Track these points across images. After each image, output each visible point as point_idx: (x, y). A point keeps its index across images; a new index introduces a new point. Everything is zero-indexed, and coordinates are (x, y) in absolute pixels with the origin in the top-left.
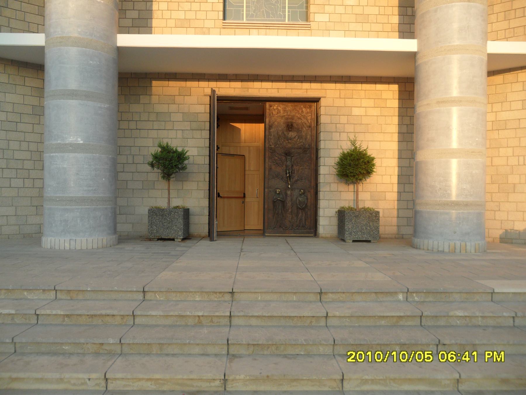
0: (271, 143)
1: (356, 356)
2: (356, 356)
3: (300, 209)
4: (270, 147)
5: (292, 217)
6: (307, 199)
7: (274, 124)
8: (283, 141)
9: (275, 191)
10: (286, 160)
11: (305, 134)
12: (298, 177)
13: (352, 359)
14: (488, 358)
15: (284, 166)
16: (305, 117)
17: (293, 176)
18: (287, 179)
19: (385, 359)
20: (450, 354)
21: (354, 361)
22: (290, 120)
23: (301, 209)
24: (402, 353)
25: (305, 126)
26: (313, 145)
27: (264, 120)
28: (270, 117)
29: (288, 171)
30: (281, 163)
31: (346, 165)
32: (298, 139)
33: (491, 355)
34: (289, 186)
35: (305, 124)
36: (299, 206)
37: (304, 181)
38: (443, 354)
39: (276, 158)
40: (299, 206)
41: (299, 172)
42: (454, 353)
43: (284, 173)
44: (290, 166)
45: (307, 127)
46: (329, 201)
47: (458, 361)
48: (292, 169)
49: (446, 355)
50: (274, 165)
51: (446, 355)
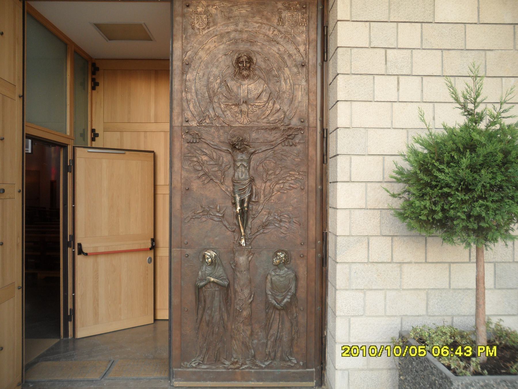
0: (189, 114)
1: (350, 350)
2: (350, 350)
3: (275, 307)
4: (185, 124)
5: (252, 331)
6: (296, 278)
7: (197, 57)
8: (222, 106)
9: (201, 257)
10: (235, 164)
11: (288, 87)
12: (269, 213)
13: (347, 354)
14: (480, 352)
15: (228, 182)
16: (289, 36)
17: (254, 212)
18: (237, 218)
19: (379, 354)
20: (443, 349)
21: (349, 355)
22: (246, 47)
23: (279, 310)
24: (396, 348)
25: (289, 63)
26: (311, 119)
27: (171, 50)
28: (184, 36)
29: (239, 195)
30: (219, 174)
31: (448, 186)
32: (268, 101)
33: (484, 349)
34: (243, 241)
35: (290, 56)
36: (274, 302)
37: (287, 225)
38: (437, 348)
39: (205, 158)
40: (274, 302)
41: (273, 198)
42: (447, 348)
43: (230, 204)
44: (247, 182)
45: (296, 66)
46: (365, 294)
47: (451, 355)
48: (251, 191)
49: (439, 350)
50: (199, 178)
51: (439, 350)
